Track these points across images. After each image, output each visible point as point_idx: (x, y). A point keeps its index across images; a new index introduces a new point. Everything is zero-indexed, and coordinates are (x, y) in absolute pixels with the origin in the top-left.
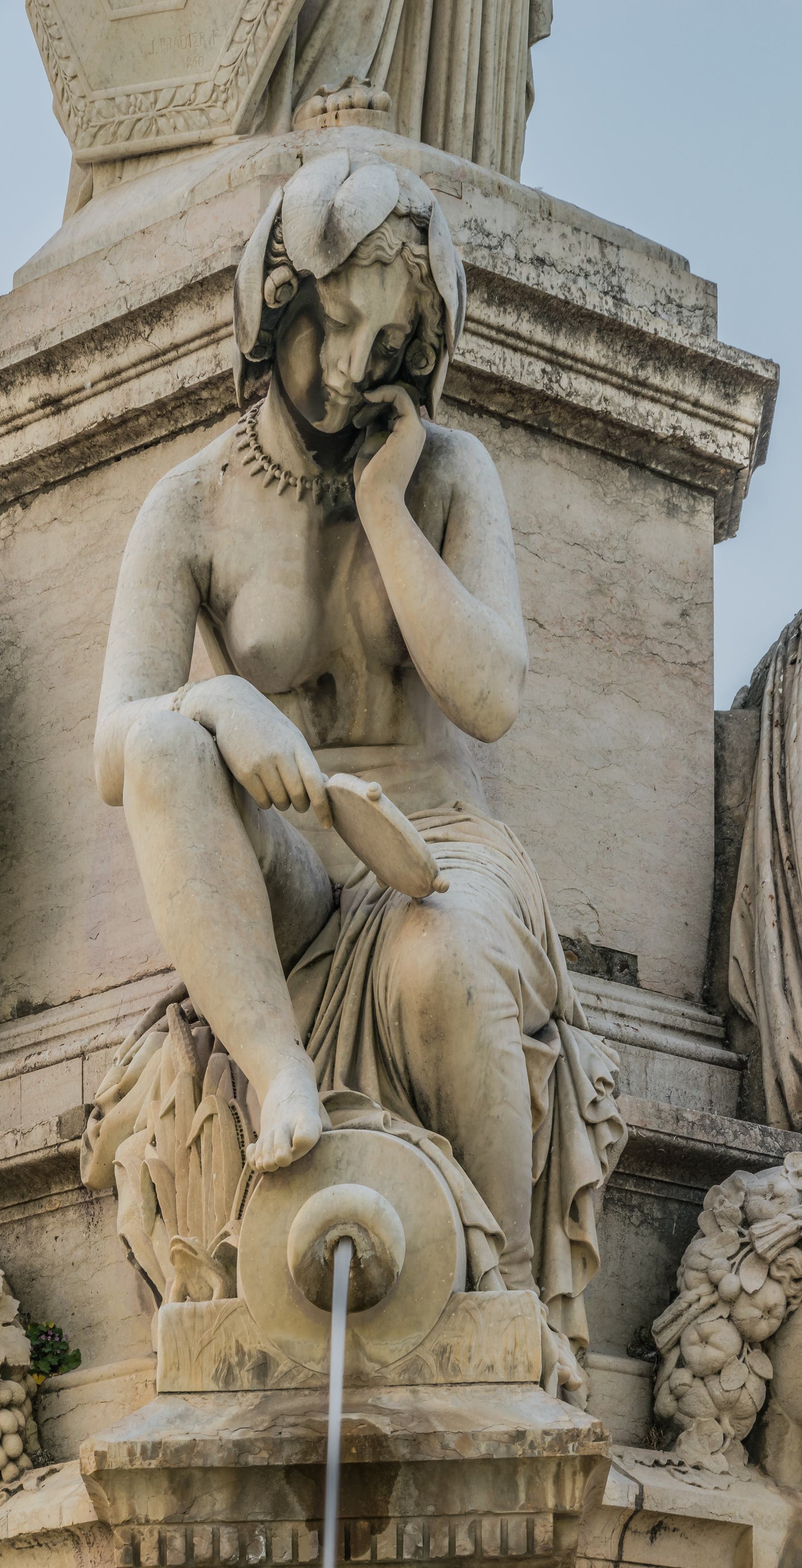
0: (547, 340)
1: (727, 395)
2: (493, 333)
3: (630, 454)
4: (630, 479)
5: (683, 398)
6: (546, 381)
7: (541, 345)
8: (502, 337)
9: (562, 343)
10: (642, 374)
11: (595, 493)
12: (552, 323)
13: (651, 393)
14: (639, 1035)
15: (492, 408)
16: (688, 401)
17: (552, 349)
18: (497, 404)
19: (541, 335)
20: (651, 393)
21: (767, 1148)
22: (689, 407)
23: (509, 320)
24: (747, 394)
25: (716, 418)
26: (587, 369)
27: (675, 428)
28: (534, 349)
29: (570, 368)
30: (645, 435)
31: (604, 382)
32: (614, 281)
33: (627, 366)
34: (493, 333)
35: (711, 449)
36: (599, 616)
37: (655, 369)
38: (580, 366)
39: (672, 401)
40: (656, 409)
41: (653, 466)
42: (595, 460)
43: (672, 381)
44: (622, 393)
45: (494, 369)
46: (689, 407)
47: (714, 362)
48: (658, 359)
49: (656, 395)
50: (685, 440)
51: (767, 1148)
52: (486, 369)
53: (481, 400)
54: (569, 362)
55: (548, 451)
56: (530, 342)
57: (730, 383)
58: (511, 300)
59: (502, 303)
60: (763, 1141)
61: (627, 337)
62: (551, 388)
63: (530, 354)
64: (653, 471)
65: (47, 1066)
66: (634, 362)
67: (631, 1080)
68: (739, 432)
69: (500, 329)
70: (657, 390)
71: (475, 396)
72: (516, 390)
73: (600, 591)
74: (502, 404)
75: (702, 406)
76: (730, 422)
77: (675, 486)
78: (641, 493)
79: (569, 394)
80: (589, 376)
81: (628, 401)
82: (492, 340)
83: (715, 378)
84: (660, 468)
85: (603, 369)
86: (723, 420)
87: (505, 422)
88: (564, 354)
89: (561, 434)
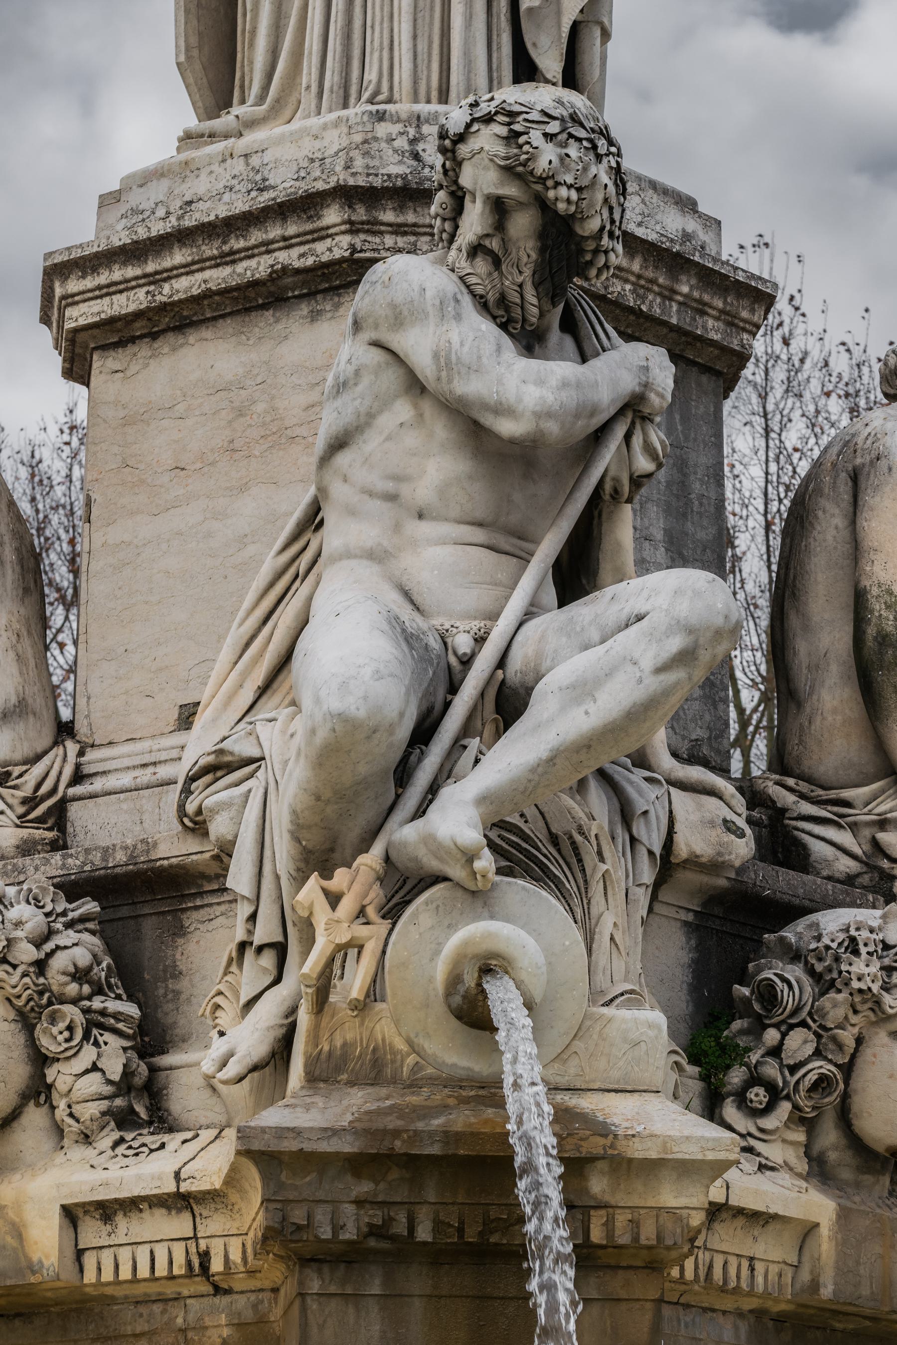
0: (138, 272)
1: (310, 218)
2: (97, 293)
3: (267, 298)
4: (273, 316)
5: (272, 242)
6: (150, 298)
7: (136, 278)
8: (105, 291)
9: (151, 267)
10: (226, 248)
11: (239, 343)
12: (139, 259)
13: (243, 254)
14: (158, 776)
15: (138, 334)
16: (278, 242)
17: (145, 276)
18: (139, 329)
19: (131, 271)
20: (243, 254)
21: (68, 869)
22: (281, 244)
23: (103, 278)
24: (328, 206)
25: (309, 237)
26: (182, 270)
27: (272, 266)
28: (134, 283)
29: (169, 278)
30: (255, 284)
31: (202, 270)
32: (258, 177)
33: (210, 250)
34: (97, 293)
35: (310, 261)
36: (239, 434)
37: (237, 238)
38: (175, 272)
39: (263, 249)
40: (253, 263)
41: (290, 294)
42: (239, 319)
43: (256, 236)
44: (220, 268)
45: (103, 316)
46: (281, 244)
47: (281, 205)
48: (238, 229)
49: (249, 253)
50: (285, 269)
51: (68, 869)
52: (98, 319)
53: (127, 334)
54: (165, 275)
55: (192, 337)
56: (127, 281)
57: (309, 208)
58: (100, 265)
59: (95, 270)
60: (64, 865)
61: (203, 232)
62: (155, 301)
63: (133, 288)
64: (295, 297)
65: (730, 808)
66: (217, 243)
67: (144, 818)
68: (336, 234)
69: (99, 288)
70: (247, 249)
71: (120, 334)
72: (138, 315)
73: (241, 415)
74: (143, 327)
75: (291, 238)
76: (324, 233)
77: (319, 297)
78: (284, 320)
79: (171, 296)
80: (187, 274)
81: (226, 271)
82: (101, 297)
83: (294, 211)
84: (296, 293)
85: (194, 263)
86: (316, 235)
87: (154, 336)
88: (157, 273)
89: (201, 318)
